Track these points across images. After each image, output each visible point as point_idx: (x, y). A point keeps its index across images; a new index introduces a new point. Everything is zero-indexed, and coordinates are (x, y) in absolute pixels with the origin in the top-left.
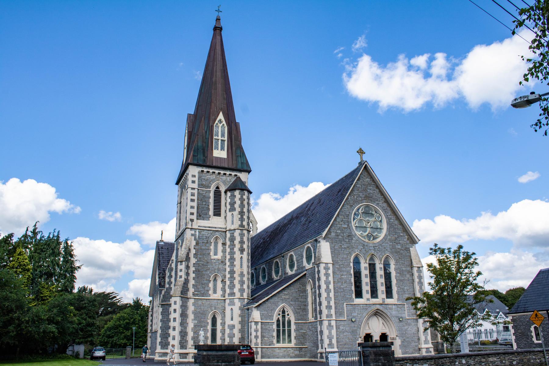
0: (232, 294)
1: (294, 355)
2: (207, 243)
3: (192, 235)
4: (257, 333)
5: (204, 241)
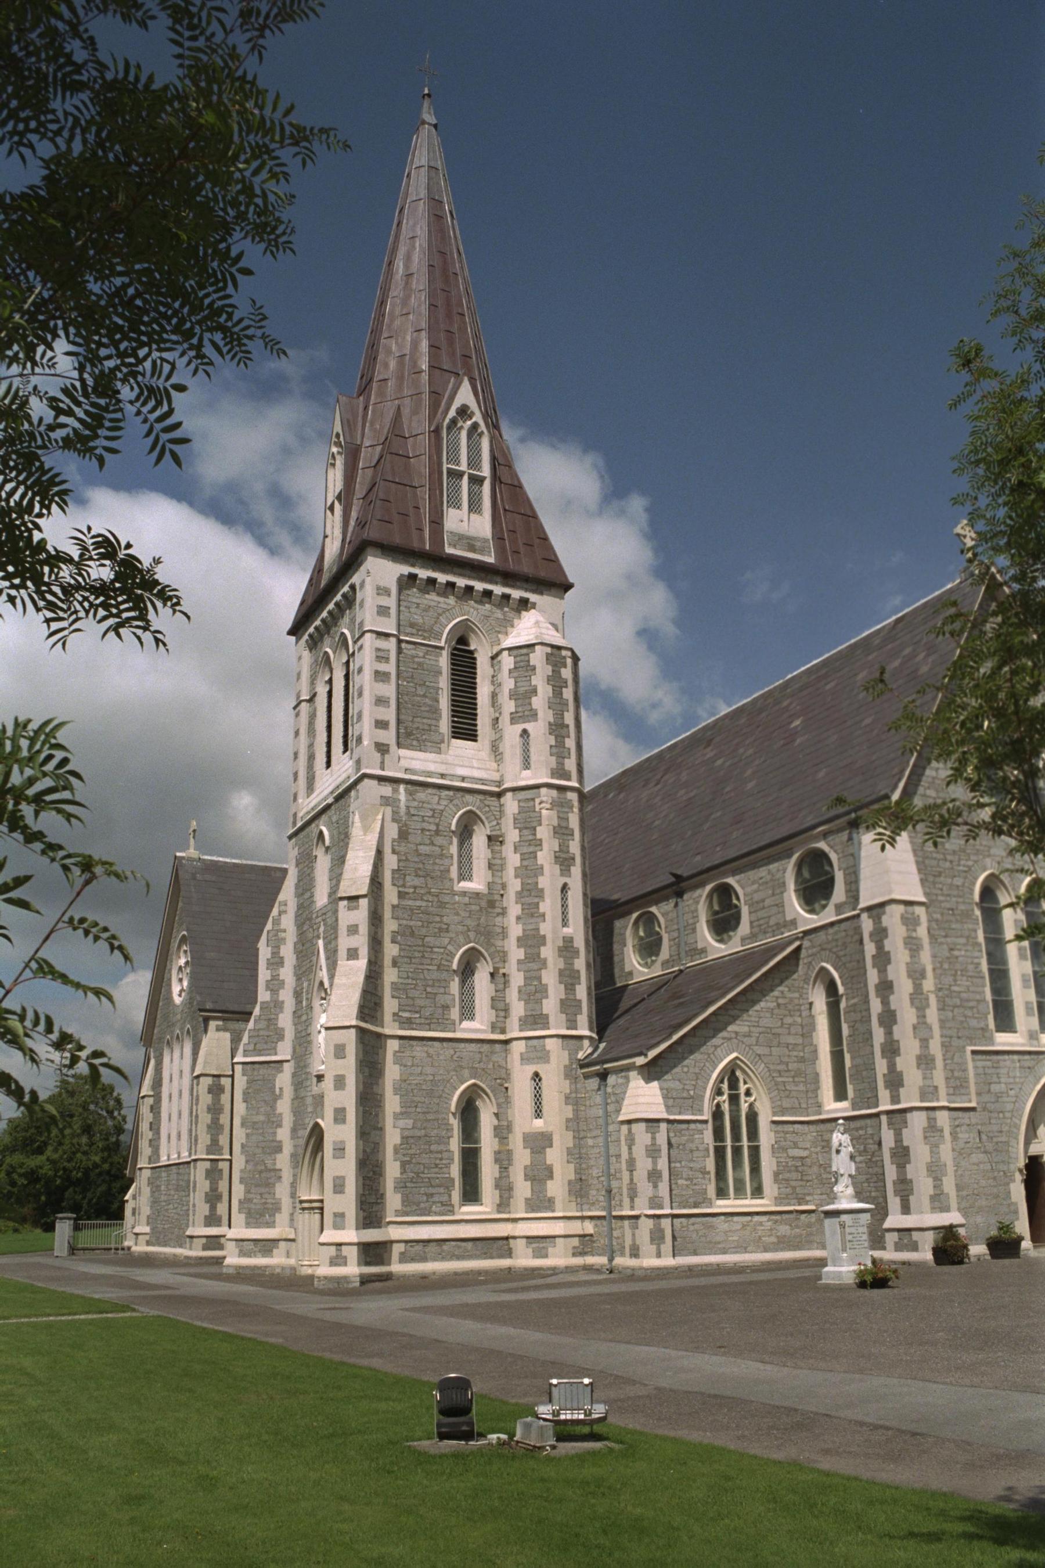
0: (535, 1019)
1: (773, 1239)
2: (437, 832)
3: (386, 801)
4: (655, 1163)
5: (425, 825)
